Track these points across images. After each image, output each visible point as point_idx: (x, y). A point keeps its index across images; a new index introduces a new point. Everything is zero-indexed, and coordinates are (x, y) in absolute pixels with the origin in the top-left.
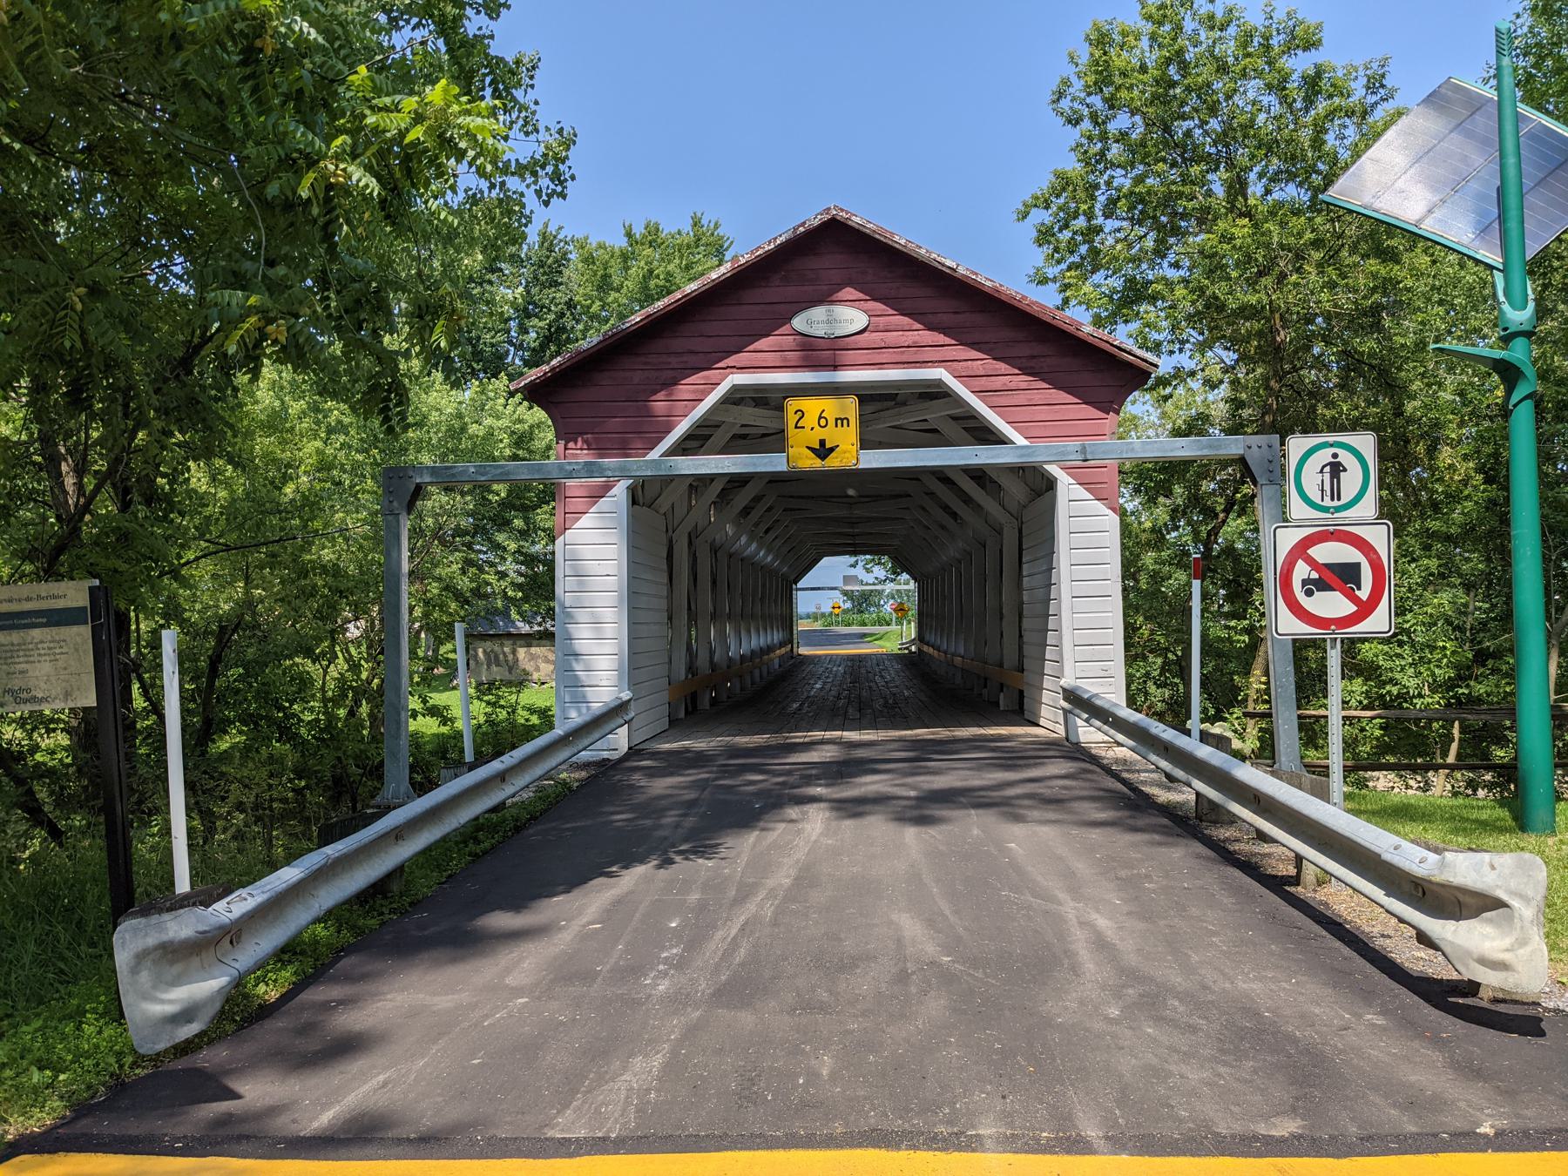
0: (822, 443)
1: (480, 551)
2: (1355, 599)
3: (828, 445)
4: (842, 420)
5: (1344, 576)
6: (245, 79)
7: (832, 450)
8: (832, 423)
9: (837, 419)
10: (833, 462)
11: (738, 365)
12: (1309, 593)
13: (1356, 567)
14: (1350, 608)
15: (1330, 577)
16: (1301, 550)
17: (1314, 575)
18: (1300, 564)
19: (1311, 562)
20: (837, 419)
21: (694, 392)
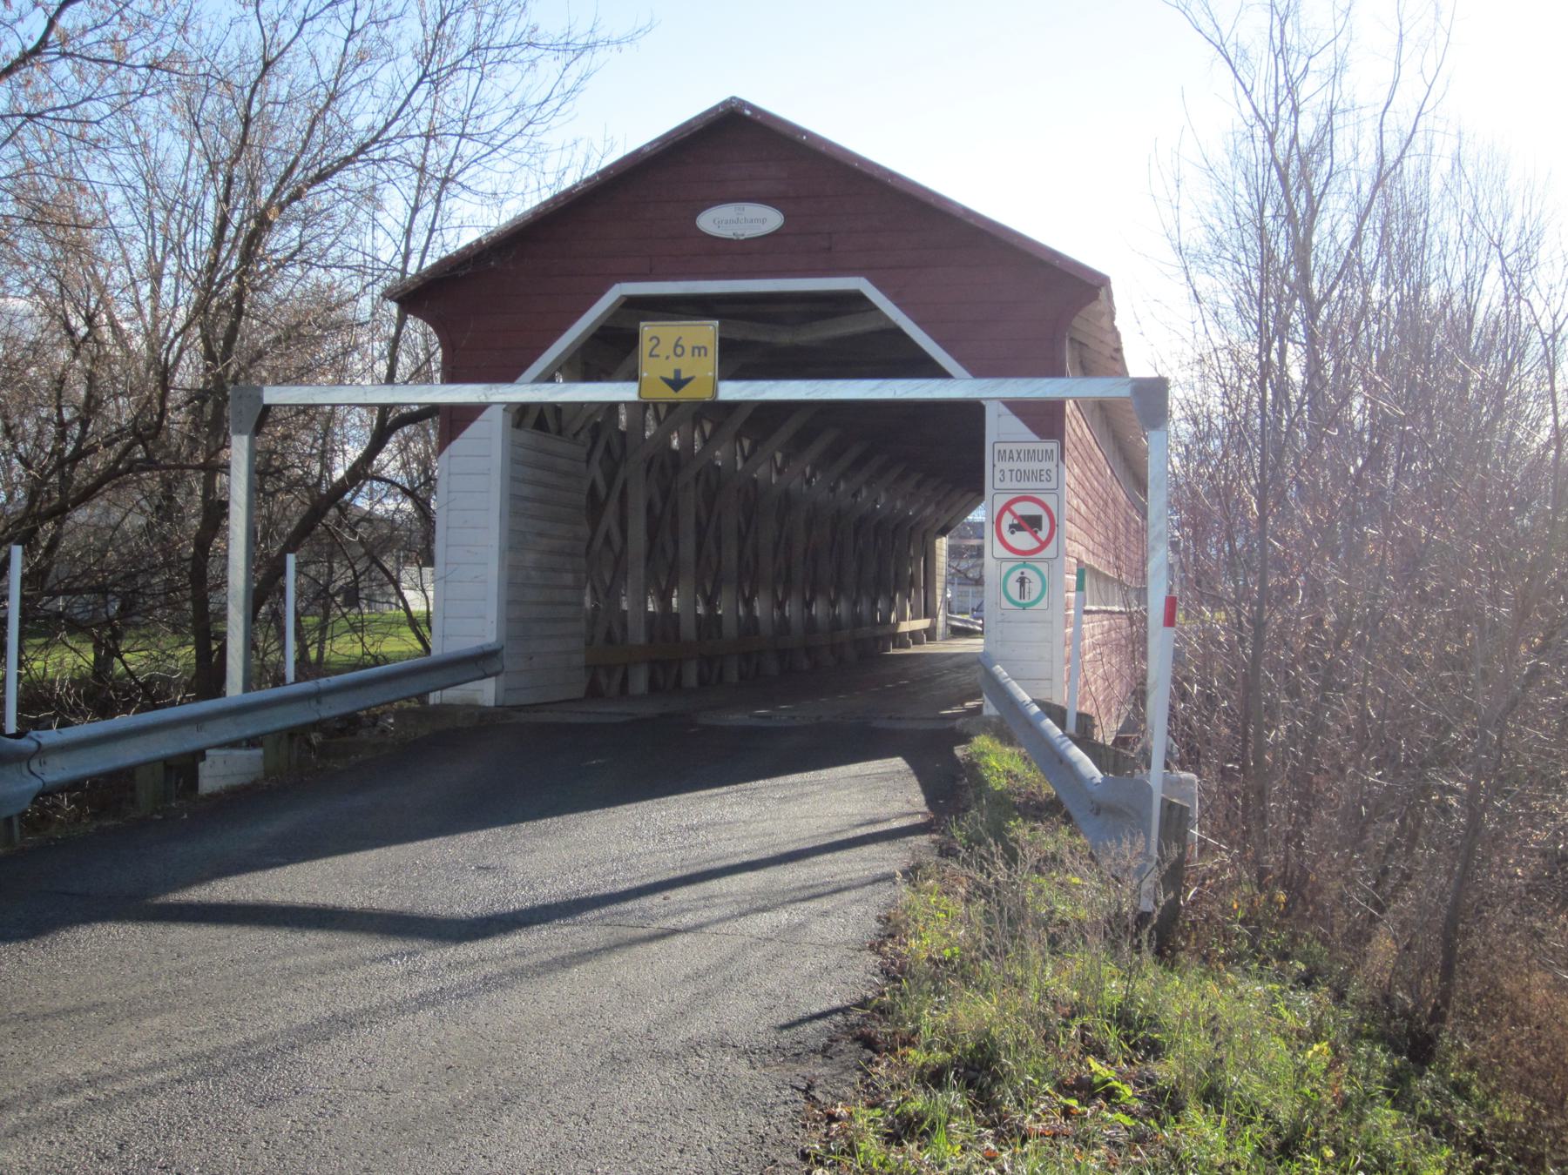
0: (678, 372)
1: (177, 783)
2: (1038, 539)
3: (684, 376)
4: (699, 348)
6: (172, 1088)
7: (688, 380)
8: (688, 350)
9: (694, 348)
10: (686, 394)
12: (1013, 533)
14: (1036, 544)
17: (1016, 522)
19: (1013, 513)
20: (694, 348)
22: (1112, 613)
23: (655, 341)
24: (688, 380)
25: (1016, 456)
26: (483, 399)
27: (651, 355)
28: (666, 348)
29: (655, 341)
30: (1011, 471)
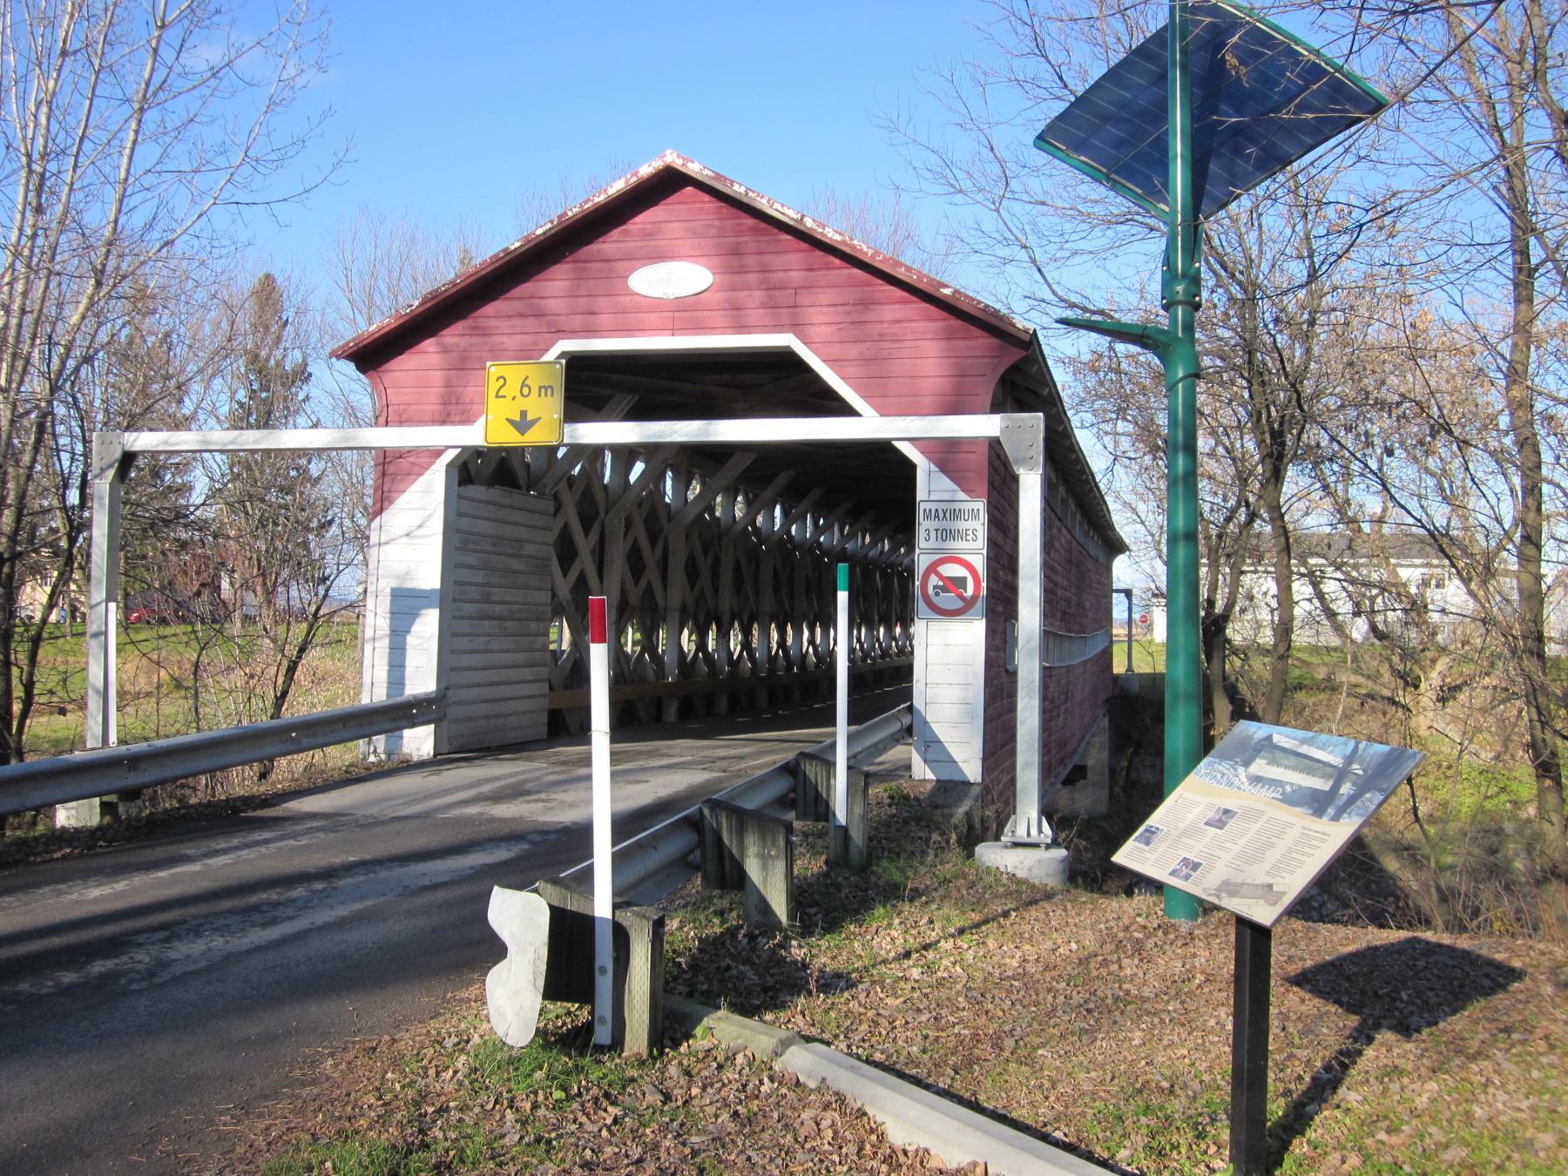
0: (524, 414)
4: (546, 388)
7: (534, 422)
17: (941, 583)
20: (540, 388)
22: (135, 142)
23: (502, 381)
24: (534, 422)
25: (941, 515)
26: (577, 574)
27: (497, 396)
28: (512, 388)
29: (502, 381)
30: (937, 530)
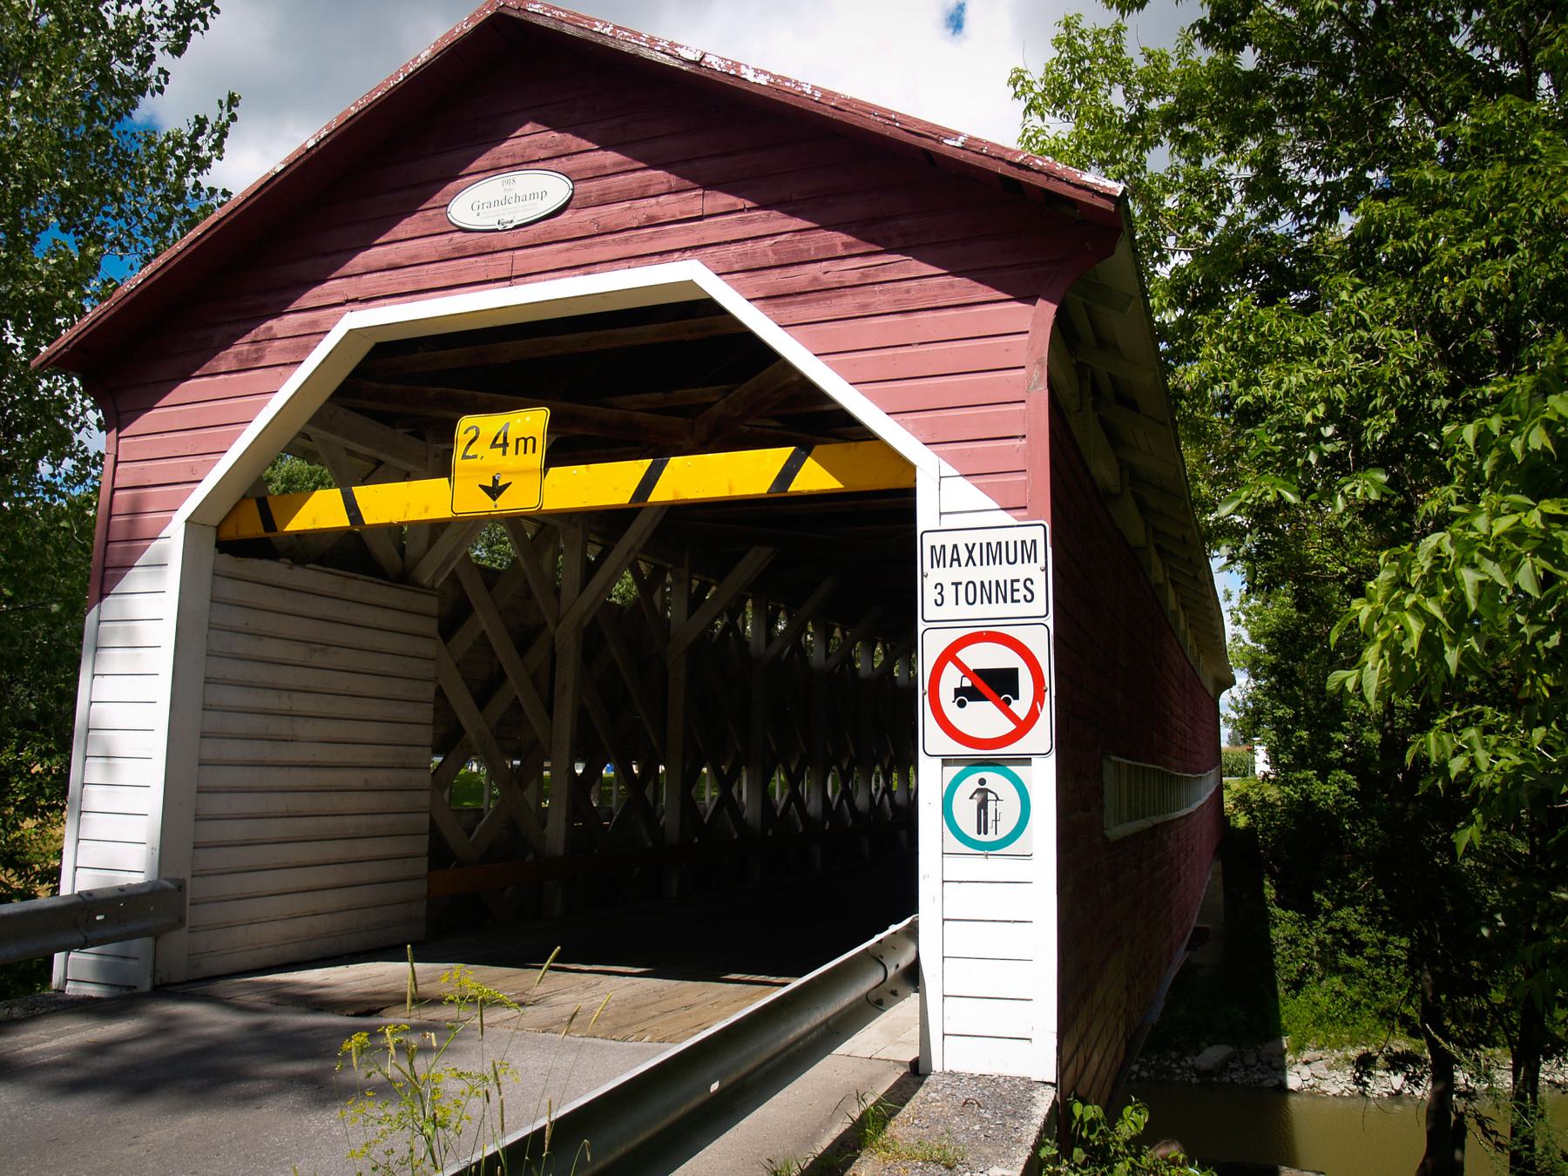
0: (495, 481)
2: (1012, 716)
5: (998, 685)
10: (509, 503)
11: (361, 296)
12: (962, 704)
13: (1012, 674)
15: (983, 687)
16: (949, 655)
17: (967, 683)
18: (950, 666)
19: (960, 665)
20: (518, 440)
21: (283, 350)
